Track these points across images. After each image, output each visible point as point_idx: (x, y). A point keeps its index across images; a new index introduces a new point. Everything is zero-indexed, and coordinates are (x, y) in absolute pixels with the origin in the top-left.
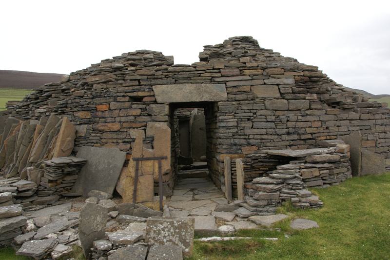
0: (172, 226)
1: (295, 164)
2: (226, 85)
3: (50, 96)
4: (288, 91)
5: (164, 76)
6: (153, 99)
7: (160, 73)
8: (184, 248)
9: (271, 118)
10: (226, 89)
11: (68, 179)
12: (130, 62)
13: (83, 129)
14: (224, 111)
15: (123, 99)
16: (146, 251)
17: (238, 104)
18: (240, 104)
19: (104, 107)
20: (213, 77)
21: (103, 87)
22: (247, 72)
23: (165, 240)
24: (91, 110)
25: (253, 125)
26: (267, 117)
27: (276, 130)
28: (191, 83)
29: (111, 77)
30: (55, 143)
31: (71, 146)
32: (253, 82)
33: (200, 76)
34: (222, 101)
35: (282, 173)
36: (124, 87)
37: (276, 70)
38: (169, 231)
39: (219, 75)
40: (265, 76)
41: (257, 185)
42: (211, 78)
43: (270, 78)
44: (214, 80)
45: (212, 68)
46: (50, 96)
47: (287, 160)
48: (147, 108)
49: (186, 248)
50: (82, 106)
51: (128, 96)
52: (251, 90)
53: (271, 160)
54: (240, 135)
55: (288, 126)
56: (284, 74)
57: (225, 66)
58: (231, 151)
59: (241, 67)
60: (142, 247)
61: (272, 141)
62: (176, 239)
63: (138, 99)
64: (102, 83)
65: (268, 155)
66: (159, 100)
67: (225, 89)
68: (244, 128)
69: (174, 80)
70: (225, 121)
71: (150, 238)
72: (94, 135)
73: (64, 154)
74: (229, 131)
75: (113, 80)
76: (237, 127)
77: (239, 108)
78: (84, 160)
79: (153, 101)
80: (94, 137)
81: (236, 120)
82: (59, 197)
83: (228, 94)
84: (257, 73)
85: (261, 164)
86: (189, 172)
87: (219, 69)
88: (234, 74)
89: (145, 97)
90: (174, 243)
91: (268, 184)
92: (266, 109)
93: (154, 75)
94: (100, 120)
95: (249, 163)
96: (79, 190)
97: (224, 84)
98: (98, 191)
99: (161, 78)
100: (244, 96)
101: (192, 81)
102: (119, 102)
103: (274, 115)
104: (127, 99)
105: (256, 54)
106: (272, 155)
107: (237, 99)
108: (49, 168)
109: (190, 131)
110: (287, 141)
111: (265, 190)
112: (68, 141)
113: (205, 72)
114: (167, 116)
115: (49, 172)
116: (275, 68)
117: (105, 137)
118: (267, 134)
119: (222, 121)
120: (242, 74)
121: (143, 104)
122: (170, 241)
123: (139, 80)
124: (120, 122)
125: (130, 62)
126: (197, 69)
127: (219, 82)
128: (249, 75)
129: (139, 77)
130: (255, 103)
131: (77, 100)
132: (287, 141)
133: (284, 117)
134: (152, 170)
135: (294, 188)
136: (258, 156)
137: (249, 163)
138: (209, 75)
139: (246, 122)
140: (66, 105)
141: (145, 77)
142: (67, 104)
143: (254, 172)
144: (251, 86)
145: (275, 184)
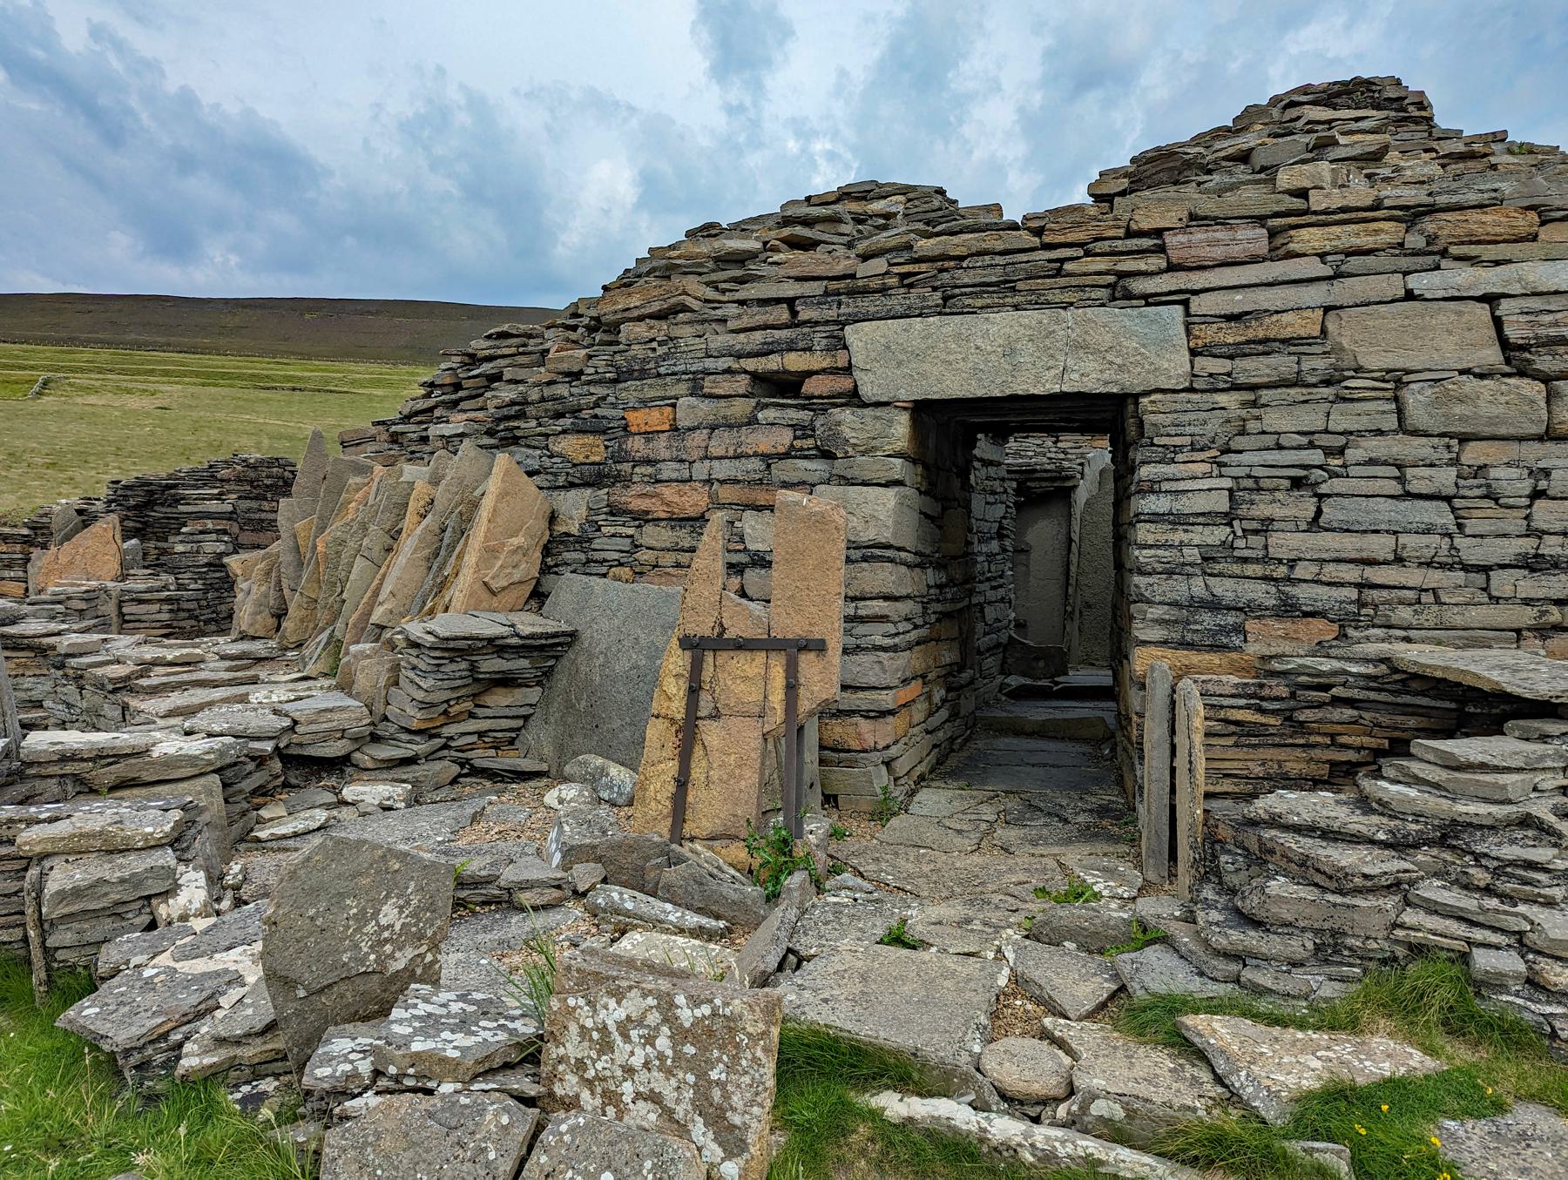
0: (665, 1020)
1: (1544, 738)
2: (1188, 314)
3: (498, 377)
4: (1553, 332)
5: (893, 281)
6: (844, 384)
7: (879, 265)
8: (720, 1152)
9: (1430, 479)
10: (1188, 332)
11: (500, 700)
12: (786, 232)
13: (575, 507)
14: (1165, 441)
15: (724, 386)
16: (521, 1132)
17: (1244, 404)
18: (1254, 404)
19: (655, 418)
20: (1122, 275)
21: (650, 335)
22: (1309, 238)
23: (627, 1088)
24: (604, 432)
25: (1319, 512)
26: (1409, 472)
27: (1458, 541)
28: (1016, 307)
29: (685, 293)
30: (460, 557)
31: (529, 568)
32: (1340, 292)
33: (1059, 273)
34: (1163, 391)
35: (1437, 786)
36: (733, 331)
37: (1484, 218)
38: (649, 1041)
39: (1156, 262)
40: (1416, 253)
41: (1268, 834)
42: (1111, 279)
43: (1444, 263)
44: (1125, 288)
45: (1121, 233)
46: (498, 377)
47: (1488, 710)
48: (818, 424)
49: (730, 1155)
50: (575, 411)
51: (746, 372)
52: (1324, 331)
53: (1407, 699)
54: (1245, 560)
55: (1540, 522)
56: (1535, 238)
57: (1193, 217)
58: (1189, 637)
59: (1277, 215)
60: (506, 1110)
61: (1427, 598)
62: (677, 1092)
63: (784, 386)
64: (652, 316)
65: (1395, 671)
66: (868, 391)
67: (1182, 329)
68: (1266, 526)
69: (939, 294)
70: (1165, 486)
71: (560, 1060)
72: (612, 530)
73: (495, 602)
74: (1185, 537)
75: (695, 305)
76: (1229, 518)
77: (1252, 426)
78: (565, 628)
79: (840, 395)
80: (608, 544)
81: (1227, 483)
82: (456, 769)
83: (1194, 353)
84: (1366, 241)
85: (1349, 713)
86: (1038, 712)
87: (1158, 233)
88: (1236, 251)
89: (810, 374)
90: (668, 1114)
91: (1331, 835)
92: (1403, 428)
93: (853, 276)
94: (637, 470)
95: (1276, 706)
96: (540, 741)
97: (1179, 309)
98: (599, 761)
99: (883, 290)
100: (1283, 364)
101: (1018, 299)
102: (711, 396)
103: (1455, 462)
104: (742, 384)
105: (1385, 149)
106: (1415, 676)
107: (1242, 380)
108: (414, 652)
109: (1075, 537)
110: (1527, 602)
111: (1304, 870)
112: (515, 552)
113: (1088, 254)
114: (898, 461)
115: (414, 668)
116: (1481, 206)
117: (653, 543)
118: (1399, 560)
119: (1152, 488)
120: (1281, 252)
121: (804, 407)
122: (654, 1098)
123: (791, 302)
124: (709, 482)
125: (786, 232)
126: (1047, 239)
127: (1149, 299)
128: (1322, 256)
129: (790, 290)
130: (1345, 400)
131: (562, 390)
132: (1527, 602)
133: (1514, 473)
134: (756, 697)
135: (1509, 886)
136: (1335, 673)
137: (1276, 706)
138: (1101, 264)
139: (1279, 495)
140: (519, 409)
141: (816, 288)
142: (526, 403)
143: (1299, 753)
144: (1327, 309)
145: (1385, 845)
